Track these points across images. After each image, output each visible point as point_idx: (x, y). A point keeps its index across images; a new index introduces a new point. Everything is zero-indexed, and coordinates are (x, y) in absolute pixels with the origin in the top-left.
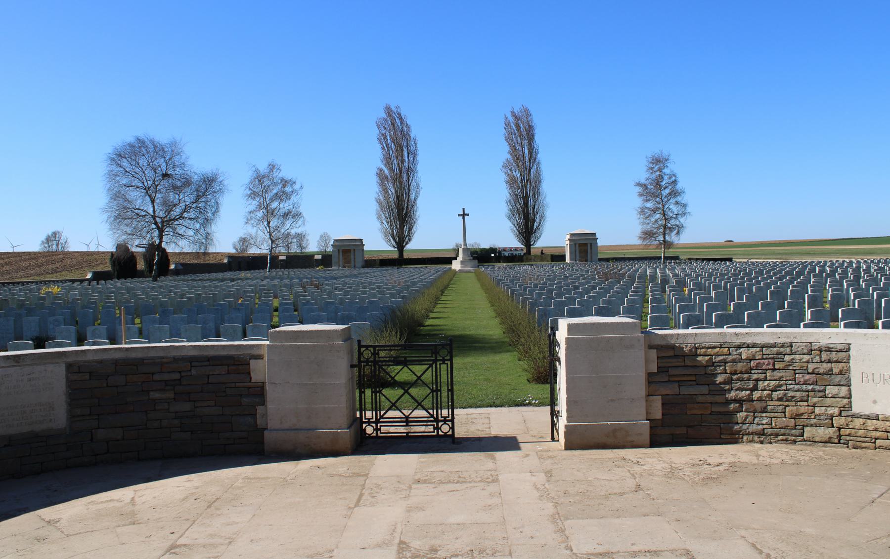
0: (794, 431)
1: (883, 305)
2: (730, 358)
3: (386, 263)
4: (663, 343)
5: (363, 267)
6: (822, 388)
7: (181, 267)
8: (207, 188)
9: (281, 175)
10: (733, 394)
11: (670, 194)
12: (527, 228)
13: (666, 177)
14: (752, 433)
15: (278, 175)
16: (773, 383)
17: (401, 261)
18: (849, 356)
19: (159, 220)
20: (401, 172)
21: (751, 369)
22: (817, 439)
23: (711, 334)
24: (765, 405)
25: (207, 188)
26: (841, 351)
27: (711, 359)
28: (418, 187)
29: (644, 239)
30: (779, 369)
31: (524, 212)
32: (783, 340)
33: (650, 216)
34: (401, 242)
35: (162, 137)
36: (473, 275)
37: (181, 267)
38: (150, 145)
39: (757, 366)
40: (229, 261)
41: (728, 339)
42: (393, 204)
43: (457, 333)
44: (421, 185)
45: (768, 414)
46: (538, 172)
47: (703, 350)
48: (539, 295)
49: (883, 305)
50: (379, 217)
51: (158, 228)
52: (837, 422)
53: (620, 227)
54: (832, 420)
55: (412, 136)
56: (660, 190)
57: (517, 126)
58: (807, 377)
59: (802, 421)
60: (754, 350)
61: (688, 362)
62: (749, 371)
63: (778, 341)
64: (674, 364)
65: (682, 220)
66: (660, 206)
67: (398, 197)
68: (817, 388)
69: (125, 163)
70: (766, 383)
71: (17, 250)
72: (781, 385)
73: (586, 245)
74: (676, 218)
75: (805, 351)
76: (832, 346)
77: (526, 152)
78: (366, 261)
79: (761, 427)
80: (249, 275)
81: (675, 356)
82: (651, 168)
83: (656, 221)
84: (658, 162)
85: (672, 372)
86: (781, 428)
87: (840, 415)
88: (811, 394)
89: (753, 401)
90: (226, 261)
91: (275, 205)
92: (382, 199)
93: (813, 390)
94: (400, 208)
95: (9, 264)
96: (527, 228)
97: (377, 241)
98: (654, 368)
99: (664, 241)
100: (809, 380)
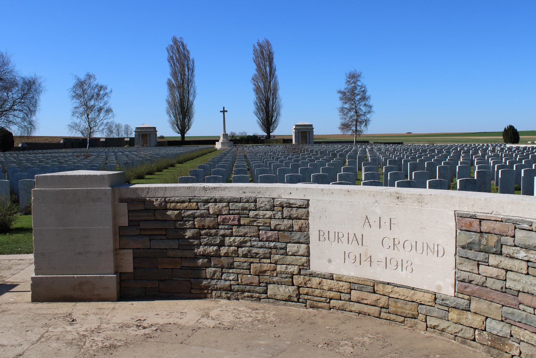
0: (258, 288)
1: (522, 175)
2: (198, 212)
3: (172, 143)
4: (134, 196)
6: (284, 245)
8: (30, 88)
9: (96, 83)
10: (201, 249)
11: (360, 99)
12: (268, 119)
13: (358, 88)
14: (220, 289)
15: (94, 83)
16: (238, 239)
17: (183, 142)
18: (308, 212)
21: (219, 225)
22: (278, 297)
23: (180, 188)
24: (231, 261)
25: (30, 88)
26: (300, 207)
27: (180, 214)
28: (195, 92)
29: (343, 129)
30: (244, 225)
32: (248, 195)
34: (183, 128)
39: (224, 222)
41: (196, 194)
45: (234, 271)
46: (276, 84)
47: (173, 204)
49: (522, 175)
50: (168, 113)
52: (298, 280)
54: (292, 278)
56: (354, 97)
57: (262, 52)
58: (270, 233)
59: (265, 278)
60: (220, 205)
61: (158, 217)
62: (216, 226)
63: (243, 196)
64: (144, 218)
65: (368, 116)
67: (181, 100)
68: (279, 245)
70: (232, 239)
72: (246, 242)
73: (306, 132)
75: (268, 207)
76: (292, 202)
77: (268, 70)
79: (228, 283)
81: (146, 210)
82: (349, 81)
83: (351, 117)
84: (354, 77)
85: (143, 225)
86: (247, 285)
87: (299, 273)
88: (274, 251)
89: (220, 256)
90: (62, 142)
91: (92, 103)
92: (170, 100)
93: (275, 248)
96: (268, 119)
97: (167, 130)
98: (124, 221)
99: (356, 130)
100: (271, 236)
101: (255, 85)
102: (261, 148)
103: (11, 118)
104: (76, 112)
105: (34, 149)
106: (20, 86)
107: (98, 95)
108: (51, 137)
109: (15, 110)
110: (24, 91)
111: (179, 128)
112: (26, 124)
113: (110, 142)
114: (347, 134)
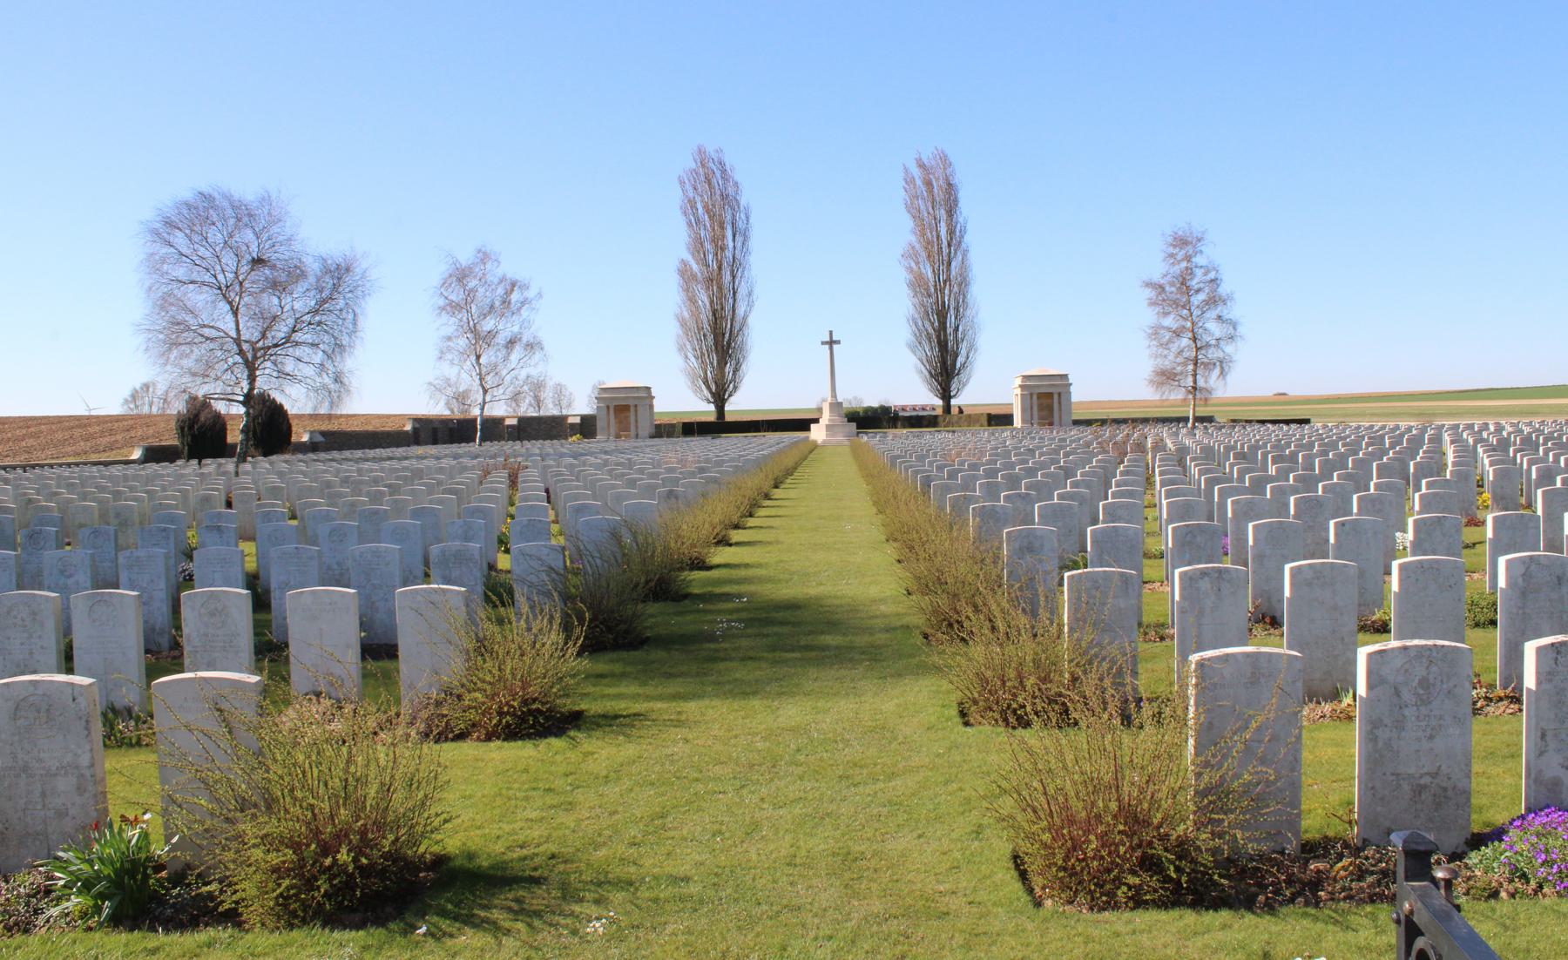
3: (692, 429)
5: (652, 437)
7: (320, 439)
8: (337, 285)
9: (499, 272)
11: (1207, 302)
12: (945, 370)
13: (1199, 272)
15: (495, 272)
17: (720, 426)
19: (245, 347)
20: (720, 268)
25: (337, 285)
28: (750, 294)
29: (1160, 385)
31: (938, 337)
33: (1170, 341)
35: (246, 189)
36: (847, 449)
37: (320, 439)
38: (226, 204)
40: (414, 429)
42: (706, 326)
43: (786, 592)
44: (757, 291)
48: (992, 491)
50: (681, 348)
51: (246, 362)
53: (1114, 367)
55: (743, 202)
57: (929, 184)
65: (1229, 349)
66: (1189, 325)
69: (179, 239)
71: (94, 413)
73: (1050, 395)
74: (1217, 346)
78: (658, 427)
80: (460, 451)
82: (1172, 255)
84: (1184, 243)
90: (408, 427)
92: (686, 315)
94: (717, 332)
95: (35, 436)
96: (945, 370)
97: (679, 396)
99: (1195, 388)
101: (910, 270)
102: (928, 437)
103: (289, 366)
104: (449, 349)
105: (340, 449)
106: (312, 279)
107: (506, 302)
108: (379, 417)
109: (297, 344)
110: (321, 292)
111: (708, 388)
112: (327, 380)
113: (529, 429)
114: (1172, 397)
